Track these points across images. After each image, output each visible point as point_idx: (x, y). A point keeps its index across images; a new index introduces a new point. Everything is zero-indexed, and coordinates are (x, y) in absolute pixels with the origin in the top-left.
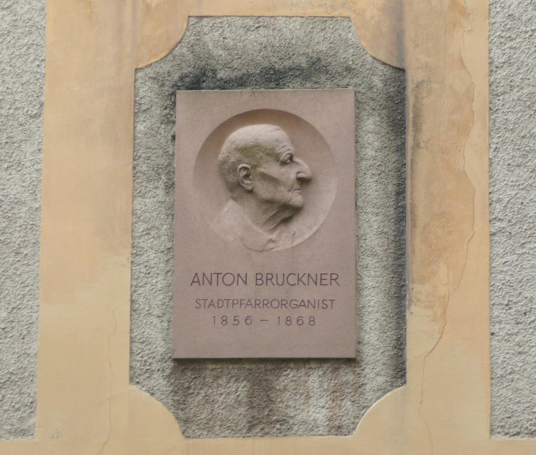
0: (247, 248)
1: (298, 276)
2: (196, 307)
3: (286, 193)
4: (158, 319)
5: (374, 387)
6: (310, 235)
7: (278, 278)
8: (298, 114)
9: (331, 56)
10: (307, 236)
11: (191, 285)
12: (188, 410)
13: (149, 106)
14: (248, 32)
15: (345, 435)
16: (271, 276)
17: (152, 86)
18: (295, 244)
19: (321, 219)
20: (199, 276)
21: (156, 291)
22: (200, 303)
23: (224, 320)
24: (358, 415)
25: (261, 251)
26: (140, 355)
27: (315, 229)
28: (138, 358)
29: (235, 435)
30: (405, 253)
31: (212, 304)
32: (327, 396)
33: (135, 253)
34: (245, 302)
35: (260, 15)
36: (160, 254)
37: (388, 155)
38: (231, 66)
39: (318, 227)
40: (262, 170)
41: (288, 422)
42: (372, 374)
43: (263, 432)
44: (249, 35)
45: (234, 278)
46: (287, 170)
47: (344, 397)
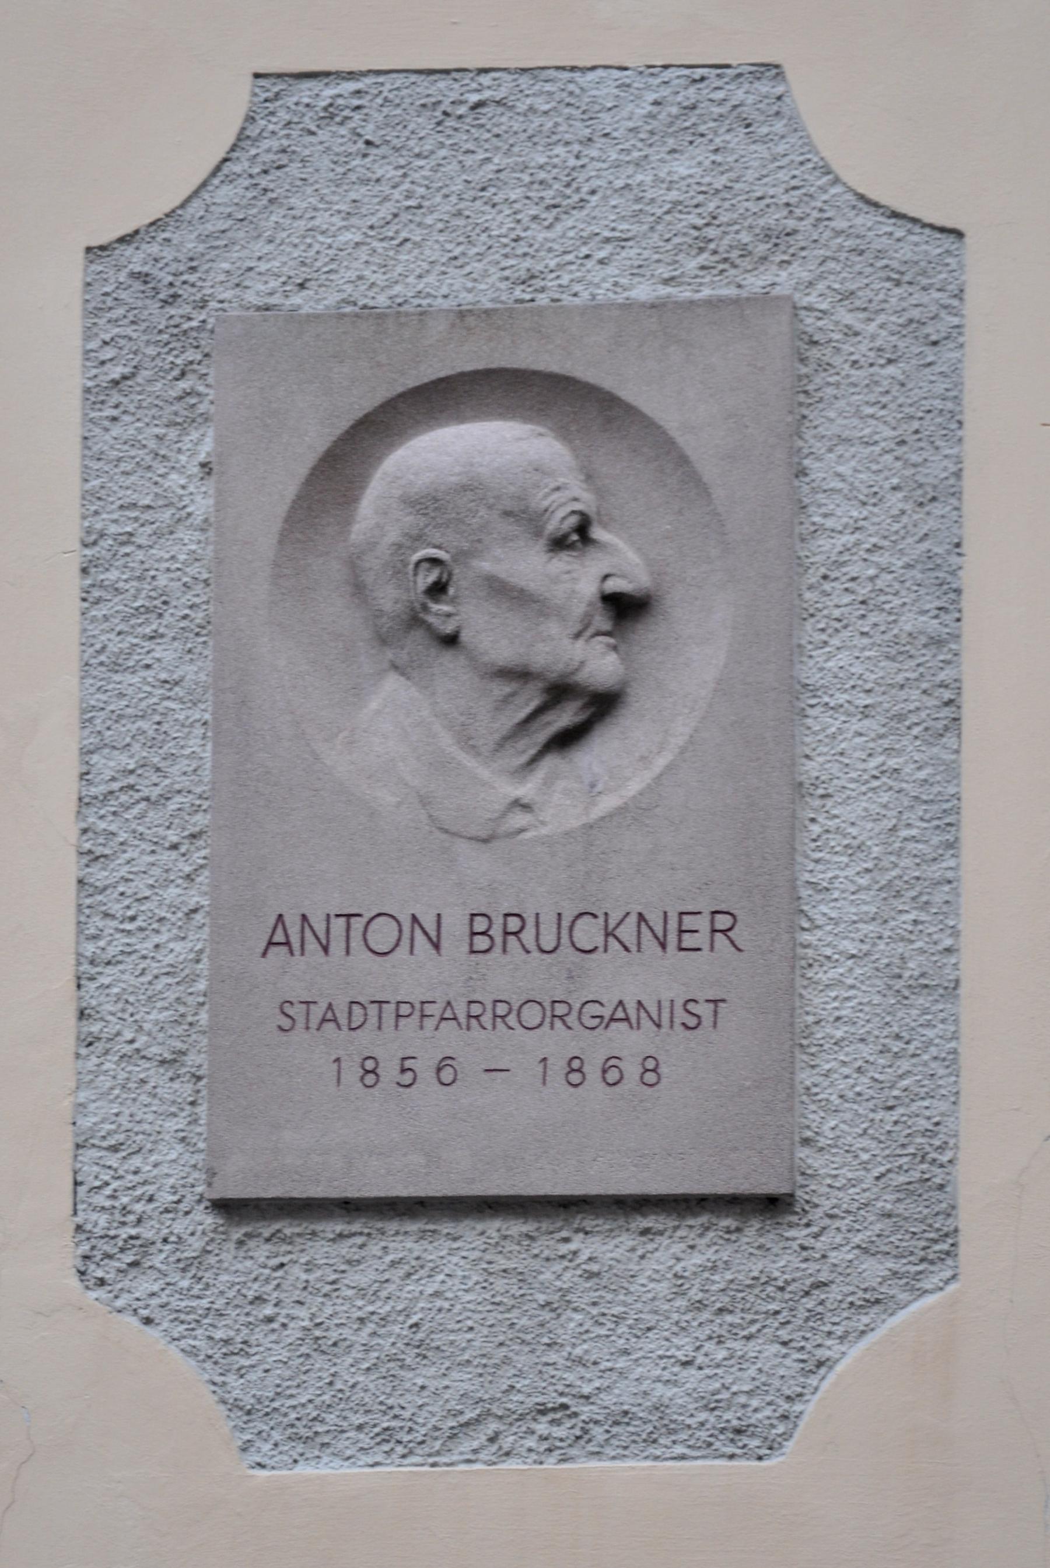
0: (440, 829)
1: (606, 921)
2: (281, 1028)
3: (566, 642)
4: (162, 1070)
5: (853, 1293)
6: (644, 785)
7: (542, 927)
8: (607, 383)
9: (717, 191)
10: (634, 787)
11: (264, 954)
13: (127, 370)
14: (447, 124)
15: (760, 1458)
17: (140, 304)
18: (596, 813)
19: (681, 730)
20: (288, 924)
21: (156, 977)
23: (368, 1072)
24: (799, 1390)
25: (485, 841)
26: (108, 1191)
27: (661, 762)
28: (100, 1200)
29: (406, 1461)
30: (957, 839)
31: (329, 1018)
32: (700, 1324)
33: (90, 852)
35: (487, 66)
36: (169, 853)
37: (903, 512)
38: (390, 234)
40: (485, 566)
41: (575, 1415)
42: (848, 1248)
43: (494, 1448)
45: (400, 931)
46: (569, 568)
47: (753, 1329)
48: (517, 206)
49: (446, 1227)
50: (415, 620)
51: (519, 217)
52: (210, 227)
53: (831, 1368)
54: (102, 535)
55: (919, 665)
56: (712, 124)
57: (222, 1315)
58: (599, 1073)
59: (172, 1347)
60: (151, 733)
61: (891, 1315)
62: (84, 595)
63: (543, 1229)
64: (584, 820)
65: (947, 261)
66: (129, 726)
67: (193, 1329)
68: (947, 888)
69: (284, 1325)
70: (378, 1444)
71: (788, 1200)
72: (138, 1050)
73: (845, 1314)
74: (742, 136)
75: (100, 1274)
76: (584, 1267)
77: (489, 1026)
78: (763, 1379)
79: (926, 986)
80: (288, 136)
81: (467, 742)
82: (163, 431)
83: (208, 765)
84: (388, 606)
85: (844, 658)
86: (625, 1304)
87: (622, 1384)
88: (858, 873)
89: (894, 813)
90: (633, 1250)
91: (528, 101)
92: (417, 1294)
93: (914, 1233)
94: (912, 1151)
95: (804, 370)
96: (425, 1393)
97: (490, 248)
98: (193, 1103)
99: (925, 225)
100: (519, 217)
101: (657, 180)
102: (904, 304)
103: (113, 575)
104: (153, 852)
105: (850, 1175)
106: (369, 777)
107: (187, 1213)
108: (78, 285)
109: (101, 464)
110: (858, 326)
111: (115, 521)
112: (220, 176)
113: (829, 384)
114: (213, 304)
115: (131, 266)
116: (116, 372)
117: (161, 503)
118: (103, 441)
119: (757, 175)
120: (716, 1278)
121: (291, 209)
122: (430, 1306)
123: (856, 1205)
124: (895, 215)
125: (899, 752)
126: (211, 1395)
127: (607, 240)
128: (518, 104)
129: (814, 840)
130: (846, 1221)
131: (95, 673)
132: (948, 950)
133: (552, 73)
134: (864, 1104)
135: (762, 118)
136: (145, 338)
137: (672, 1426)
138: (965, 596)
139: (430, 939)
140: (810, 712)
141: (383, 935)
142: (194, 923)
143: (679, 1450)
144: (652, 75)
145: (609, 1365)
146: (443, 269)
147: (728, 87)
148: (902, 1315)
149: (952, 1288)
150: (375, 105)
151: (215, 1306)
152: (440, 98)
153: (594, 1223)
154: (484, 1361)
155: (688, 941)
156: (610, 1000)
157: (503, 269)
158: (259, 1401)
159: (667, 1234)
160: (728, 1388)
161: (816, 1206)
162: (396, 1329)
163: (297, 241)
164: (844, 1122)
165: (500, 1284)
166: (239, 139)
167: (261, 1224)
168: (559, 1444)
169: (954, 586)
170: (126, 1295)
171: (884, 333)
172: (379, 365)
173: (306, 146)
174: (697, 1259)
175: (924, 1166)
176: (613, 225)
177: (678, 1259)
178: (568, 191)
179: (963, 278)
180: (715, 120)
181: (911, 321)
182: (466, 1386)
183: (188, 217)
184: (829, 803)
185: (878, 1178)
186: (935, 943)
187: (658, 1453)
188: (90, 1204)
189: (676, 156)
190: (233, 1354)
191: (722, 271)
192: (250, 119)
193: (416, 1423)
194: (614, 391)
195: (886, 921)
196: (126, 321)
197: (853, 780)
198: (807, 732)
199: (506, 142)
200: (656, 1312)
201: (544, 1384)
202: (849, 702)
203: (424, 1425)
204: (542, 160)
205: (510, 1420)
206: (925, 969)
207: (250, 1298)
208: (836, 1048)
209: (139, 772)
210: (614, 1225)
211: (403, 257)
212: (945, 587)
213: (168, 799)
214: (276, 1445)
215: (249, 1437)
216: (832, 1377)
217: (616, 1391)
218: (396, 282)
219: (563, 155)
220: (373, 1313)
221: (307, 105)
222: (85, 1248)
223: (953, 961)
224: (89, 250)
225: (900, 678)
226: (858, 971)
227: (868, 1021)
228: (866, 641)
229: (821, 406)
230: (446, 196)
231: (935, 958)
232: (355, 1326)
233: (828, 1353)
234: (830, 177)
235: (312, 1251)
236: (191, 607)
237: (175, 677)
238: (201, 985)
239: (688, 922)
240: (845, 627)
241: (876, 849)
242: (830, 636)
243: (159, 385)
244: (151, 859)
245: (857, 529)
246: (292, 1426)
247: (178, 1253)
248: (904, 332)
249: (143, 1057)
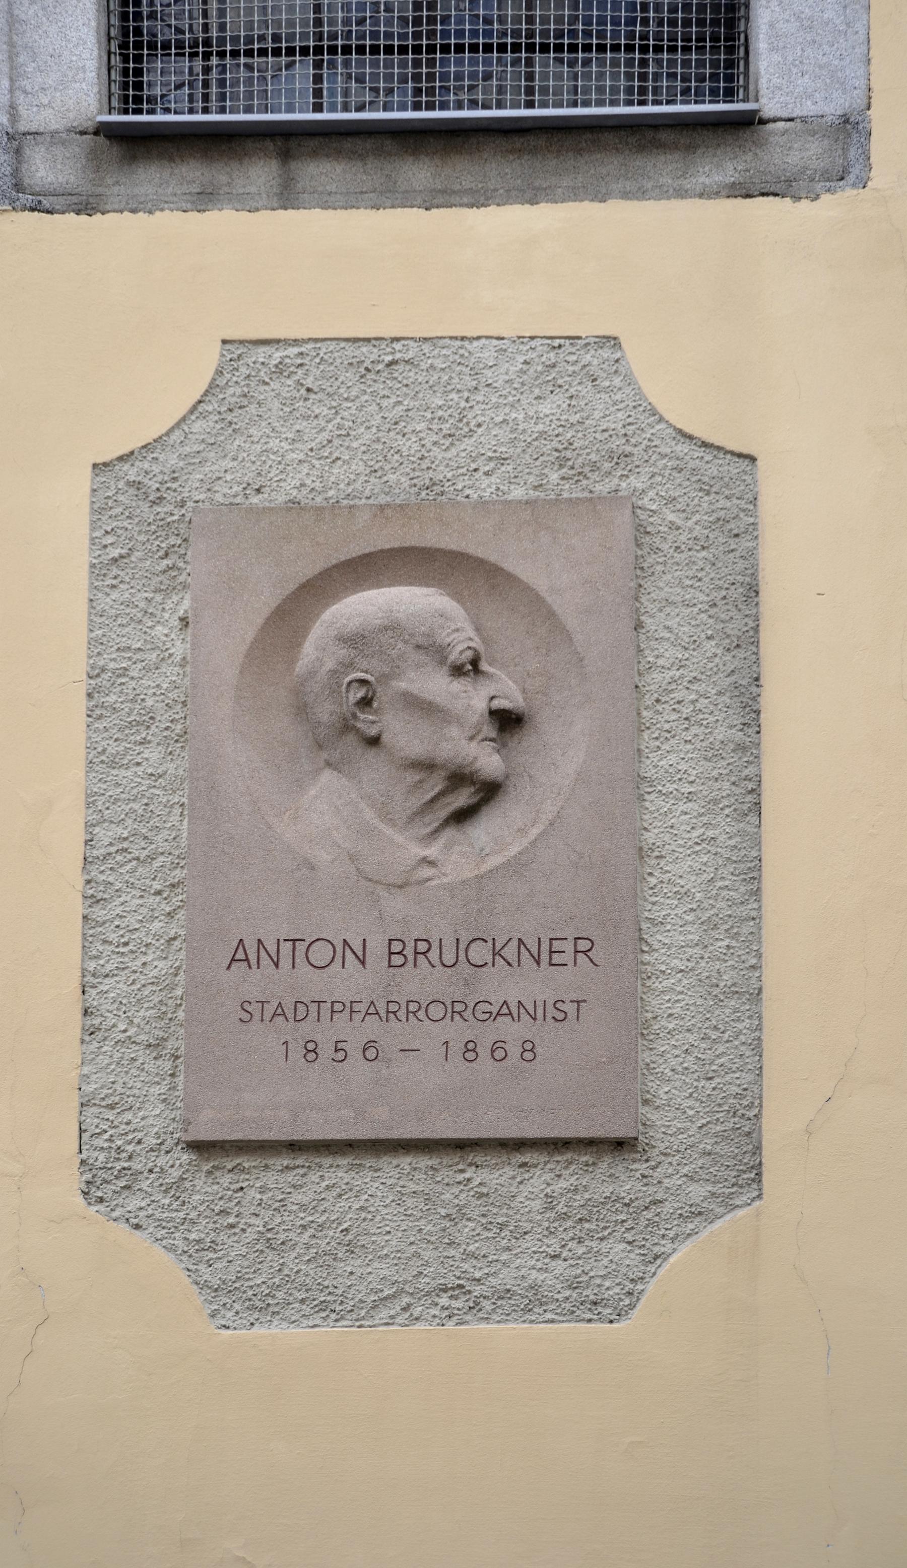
1: (494, 944)
3: (464, 742)
5: (682, 1208)
8: (493, 558)
10: (514, 850)
11: (229, 968)
12: (225, 1264)
13: (123, 551)
15: (611, 1322)
16: (427, 946)
18: (485, 868)
22: (250, 1010)
24: (641, 1275)
25: (400, 887)
26: (106, 1136)
27: (534, 832)
30: (759, 889)
32: (565, 1230)
33: (92, 896)
34: (362, 1007)
35: (399, 335)
36: (153, 897)
38: (326, 454)
39: (542, 828)
40: (403, 685)
41: (470, 1292)
43: (407, 1315)
44: (369, 383)
45: (334, 951)
47: (606, 1233)
48: (421, 435)
49: (369, 1162)
50: (347, 727)
51: (423, 442)
52: (188, 449)
53: (665, 1259)
54: (103, 670)
55: (729, 764)
56: (567, 379)
57: (194, 1223)
58: (489, 1052)
59: (157, 1244)
60: (140, 811)
61: (710, 1223)
62: (89, 712)
63: (445, 1163)
64: (476, 872)
65: (744, 478)
66: (123, 807)
67: (172, 1233)
68: (752, 923)
69: (243, 1230)
70: (317, 1312)
71: (632, 1143)
72: (130, 1037)
73: (676, 1222)
74: (589, 387)
75: (100, 1194)
76: (475, 1189)
77: (404, 1020)
78: (614, 1267)
79: (737, 992)
80: (248, 385)
81: (386, 816)
82: (151, 595)
83: (185, 835)
84: (325, 718)
85: (673, 758)
86: (507, 1215)
87: (505, 1271)
88: (685, 912)
89: (712, 869)
90: (513, 1178)
91: (430, 361)
92: (347, 1209)
93: (728, 1166)
94: (727, 1108)
95: (640, 553)
96: (353, 1277)
97: (401, 464)
98: (172, 1075)
99: (727, 452)
100: (423, 442)
101: (527, 418)
102: (714, 507)
103: (112, 698)
104: (142, 897)
105: (679, 1125)
106: (310, 842)
107: (167, 1152)
108: (87, 489)
109: (103, 619)
110: (679, 522)
111: (114, 660)
112: (196, 414)
113: (658, 563)
114: (190, 504)
115: (128, 477)
116: (115, 553)
117: (148, 647)
118: (104, 602)
119: (602, 415)
120: (578, 1197)
121: (251, 436)
122: (356, 1217)
123: (684, 1146)
124: (705, 445)
125: (715, 827)
126: (187, 1278)
127: (491, 459)
128: (421, 363)
129: (652, 888)
130: (677, 1158)
131: (97, 768)
132: (753, 967)
133: (448, 341)
134: (690, 1075)
135: (605, 375)
136: (137, 529)
137: (544, 1300)
138: (762, 715)
139: (357, 957)
140: (647, 797)
141: (321, 954)
142: (174, 947)
143: (549, 1316)
144: (523, 343)
145: (495, 1257)
146: (366, 478)
147: (578, 353)
148: (719, 1224)
149: (757, 1203)
150: (313, 364)
151: (189, 1217)
152: (363, 358)
153: (484, 1159)
154: (399, 1255)
155: (556, 958)
156: (497, 1001)
157: (412, 479)
158: (224, 1282)
159: (540, 1167)
160: (587, 1274)
161: (654, 1147)
162: (331, 1233)
163: (254, 459)
164: (675, 1088)
165: (410, 1202)
166: (210, 387)
167: (225, 1159)
168: (456, 1312)
169: (755, 708)
170: (120, 1209)
171: (698, 527)
172: (318, 544)
173: (262, 392)
174: (563, 1184)
175: (736, 1119)
176: (494, 448)
177: (548, 1184)
178: (461, 425)
179: (756, 489)
180: (570, 376)
181: (719, 519)
182: (386, 1272)
183: (172, 442)
184: (663, 862)
185: (700, 1128)
186: (743, 962)
187: (533, 1318)
188: (92, 1146)
189: (541, 401)
190: (203, 1249)
191: (577, 481)
192: (219, 372)
193: (346, 1298)
194: (498, 564)
195: (706, 946)
196: (124, 517)
197: (680, 846)
198: (646, 812)
199: (413, 390)
200: (531, 1221)
201: (445, 1271)
202: (676, 790)
203: (352, 1299)
204: (440, 403)
205: (419, 1295)
206: (736, 980)
207: (216, 1211)
208: (669, 1036)
209: (132, 839)
210: (499, 1161)
211: (335, 471)
212: (748, 709)
213: (153, 859)
214: (237, 1313)
215: (216, 1307)
216: (666, 1266)
217: (501, 1276)
218: (331, 488)
219: (456, 399)
220: (312, 1222)
221: (263, 363)
222: (88, 1176)
223: (757, 975)
224: (95, 466)
225: (715, 773)
226: (685, 982)
227: (693, 1017)
228: (689, 747)
229: (652, 579)
230: (368, 428)
231: (742, 973)
232: (299, 1231)
233: (663, 1249)
234: (657, 417)
235: (265, 1179)
236: (172, 721)
237: (159, 771)
238: (179, 992)
239: (557, 945)
240: (674, 737)
241: (698, 895)
242: (662, 743)
243: (148, 563)
244: (141, 901)
245: (681, 666)
246: (250, 1300)
247: (161, 1180)
248: (713, 527)
249: (134, 1042)
